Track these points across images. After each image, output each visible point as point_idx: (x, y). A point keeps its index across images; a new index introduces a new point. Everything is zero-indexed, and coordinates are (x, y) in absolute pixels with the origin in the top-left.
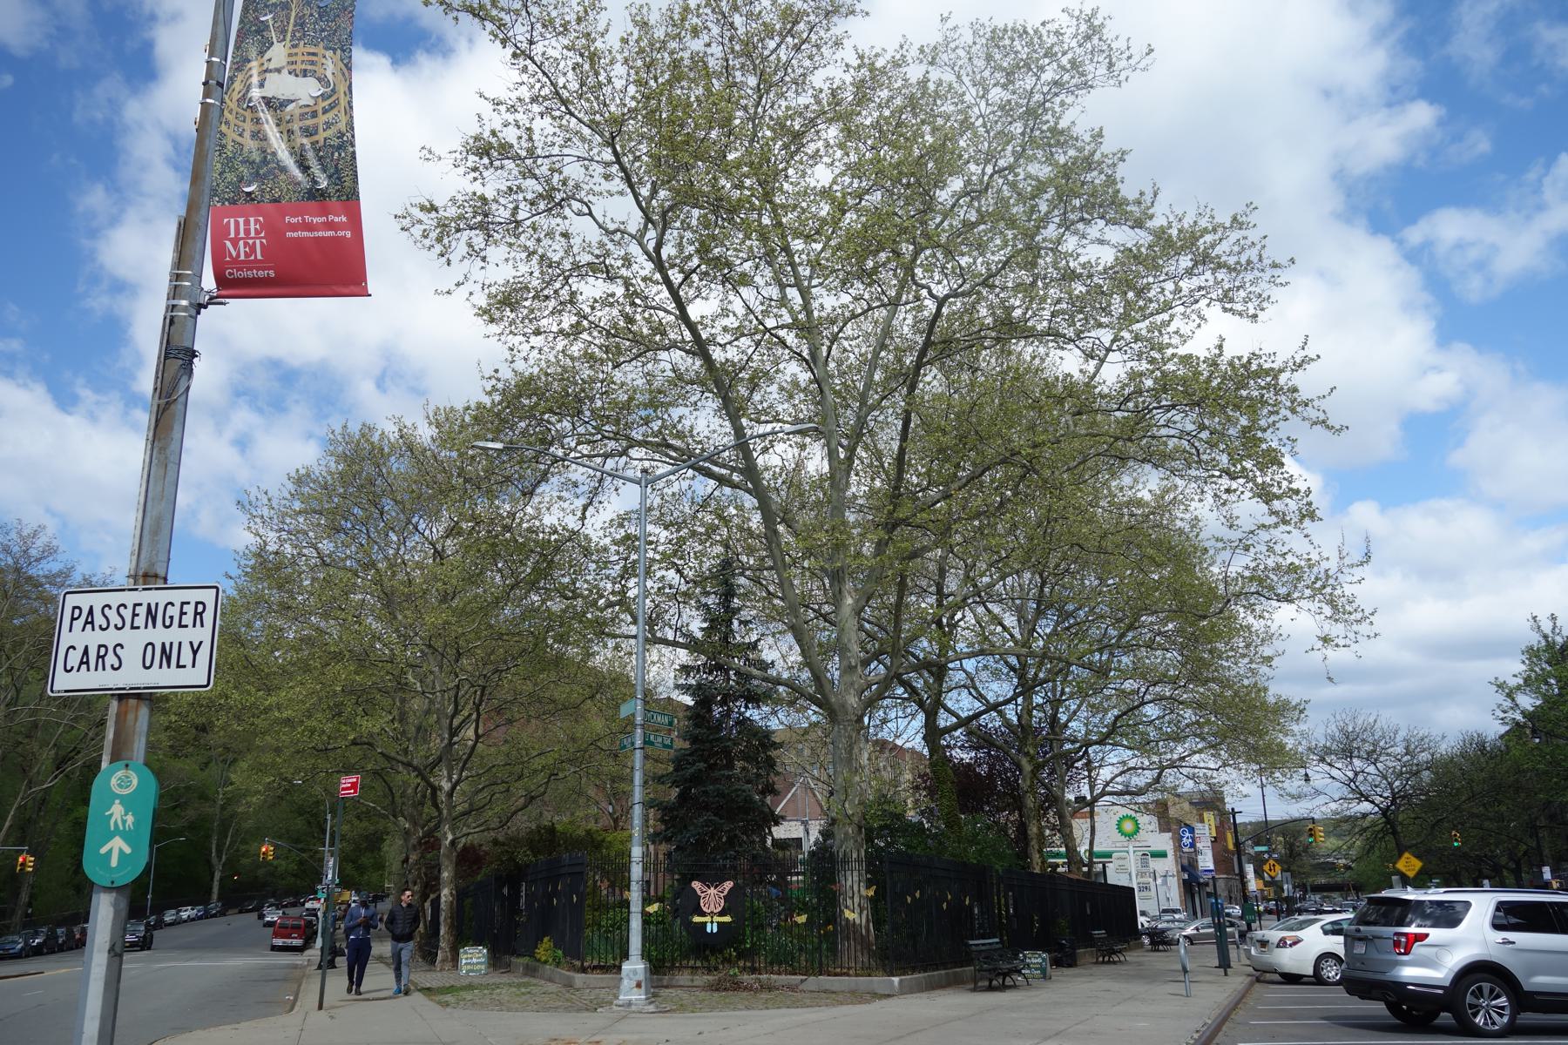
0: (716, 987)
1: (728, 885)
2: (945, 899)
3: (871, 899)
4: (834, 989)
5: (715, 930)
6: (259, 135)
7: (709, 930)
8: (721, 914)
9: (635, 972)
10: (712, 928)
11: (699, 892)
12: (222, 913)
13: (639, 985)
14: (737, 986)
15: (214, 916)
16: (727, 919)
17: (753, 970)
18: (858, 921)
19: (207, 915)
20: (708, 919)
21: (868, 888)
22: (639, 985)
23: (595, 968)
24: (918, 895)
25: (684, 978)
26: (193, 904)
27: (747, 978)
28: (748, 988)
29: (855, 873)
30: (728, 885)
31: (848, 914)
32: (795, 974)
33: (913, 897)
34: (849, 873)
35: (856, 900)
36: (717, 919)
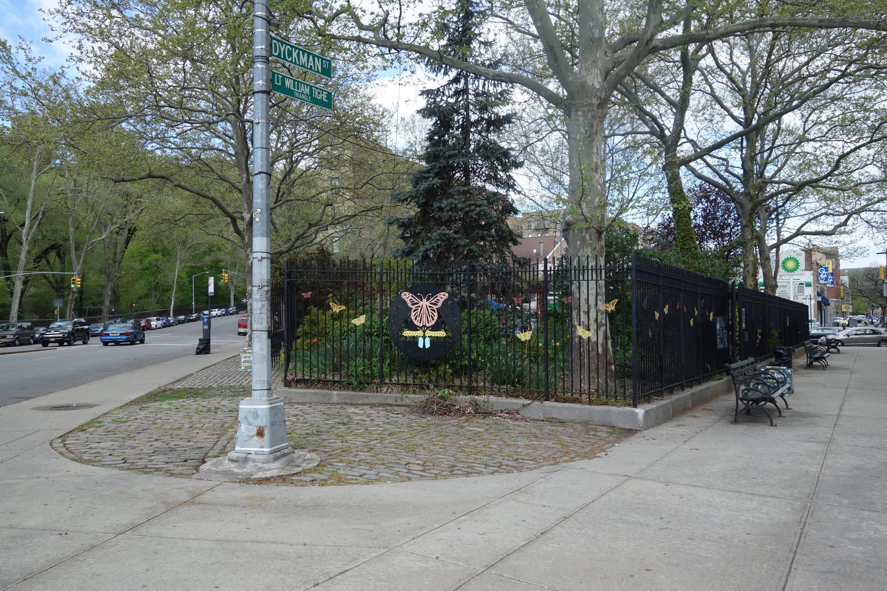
0: (424, 409)
1: (443, 296)
2: (693, 315)
3: (611, 316)
4: (561, 417)
5: (428, 345)
6: (615, 352)
7: (421, 345)
8: (434, 328)
9: (255, 414)
10: (424, 343)
11: (410, 305)
12: (237, 313)
13: (260, 433)
14: (446, 409)
15: (232, 314)
16: (441, 334)
17: (472, 390)
18: (594, 339)
19: (227, 314)
20: (419, 333)
21: (608, 301)
22: (260, 433)
23: (298, 381)
24: (666, 310)
25: (391, 395)
26: (220, 308)
27: (463, 399)
28: (460, 412)
29: (592, 284)
30: (443, 296)
31: (581, 332)
32: (517, 397)
33: (662, 313)
34: (584, 284)
35: (593, 314)
36: (429, 333)
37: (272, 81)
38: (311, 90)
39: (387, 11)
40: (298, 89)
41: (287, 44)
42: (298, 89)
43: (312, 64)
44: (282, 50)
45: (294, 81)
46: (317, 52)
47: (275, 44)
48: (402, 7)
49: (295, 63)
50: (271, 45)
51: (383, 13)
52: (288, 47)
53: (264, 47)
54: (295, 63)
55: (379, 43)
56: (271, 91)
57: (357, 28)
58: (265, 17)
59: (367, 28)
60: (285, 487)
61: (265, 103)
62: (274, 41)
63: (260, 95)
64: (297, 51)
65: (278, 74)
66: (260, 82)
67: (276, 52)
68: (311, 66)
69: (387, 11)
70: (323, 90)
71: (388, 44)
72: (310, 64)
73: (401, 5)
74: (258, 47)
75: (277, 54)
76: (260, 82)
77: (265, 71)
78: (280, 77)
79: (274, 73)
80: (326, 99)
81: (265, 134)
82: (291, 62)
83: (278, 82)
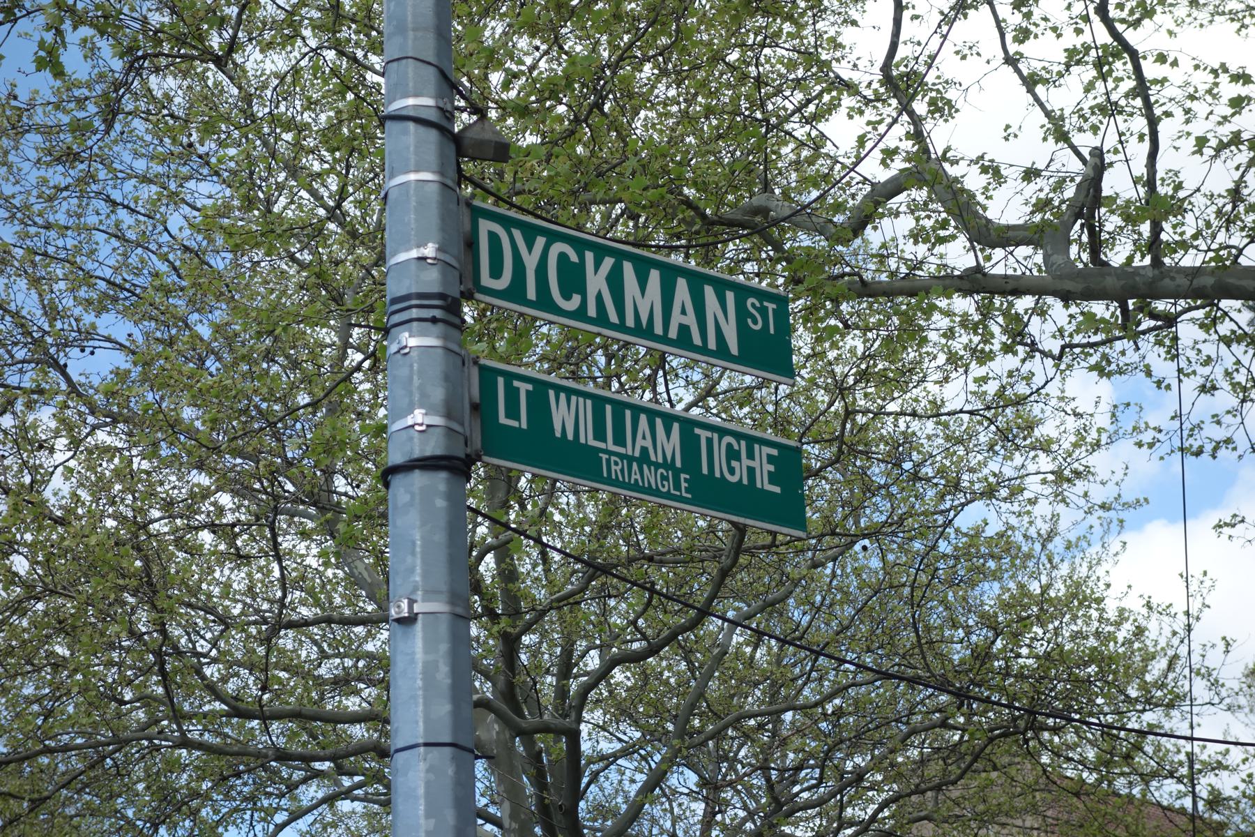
37: (482, 409)
38: (690, 444)
39: (1098, 153)
40: (620, 440)
41: (553, 237)
42: (620, 440)
43: (691, 320)
44: (531, 261)
45: (599, 402)
46: (564, 57)
47: (493, 237)
48: (1162, 127)
49: (602, 320)
50: (471, 244)
51: (1075, 166)
52: (558, 248)
53: (430, 250)
54: (602, 320)
55: (1069, 285)
56: (470, 461)
57: (962, 240)
58: (433, 116)
59: (1006, 237)
60: (400, 800)
61: (442, 521)
62: (485, 226)
63: (418, 478)
64: (608, 262)
65: (510, 376)
66: (418, 416)
67: (496, 273)
68: (684, 329)
69: (1098, 153)
70: (751, 440)
71: (1110, 282)
72: (676, 319)
73: (1153, 123)
74: (402, 257)
75: (503, 283)
76: (418, 416)
77: (437, 365)
78: (524, 387)
79: (488, 375)
80: (773, 478)
81: (443, 671)
82: (580, 314)
83: (513, 413)
